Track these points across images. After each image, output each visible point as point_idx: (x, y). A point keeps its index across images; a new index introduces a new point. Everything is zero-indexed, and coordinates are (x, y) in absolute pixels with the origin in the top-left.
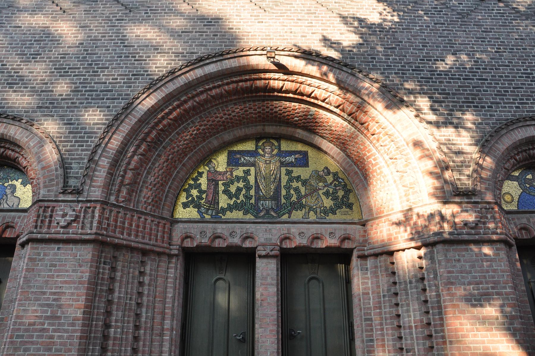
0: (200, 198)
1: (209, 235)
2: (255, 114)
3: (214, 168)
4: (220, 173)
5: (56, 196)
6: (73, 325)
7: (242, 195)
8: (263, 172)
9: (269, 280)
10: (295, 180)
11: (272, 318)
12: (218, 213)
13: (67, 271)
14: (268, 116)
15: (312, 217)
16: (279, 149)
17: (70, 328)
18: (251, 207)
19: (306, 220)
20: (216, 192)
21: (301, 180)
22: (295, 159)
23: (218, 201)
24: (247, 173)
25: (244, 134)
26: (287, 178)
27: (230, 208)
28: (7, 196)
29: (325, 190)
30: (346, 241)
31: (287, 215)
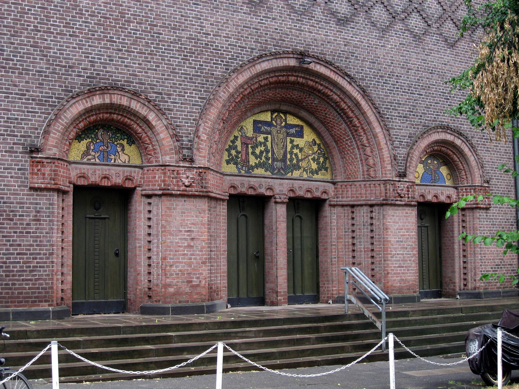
0: (237, 157)
1: (246, 186)
2: (280, 97)
4: (249, 138)
5: (177, 162)
6: (202, 251)
12: (249, 169)
13: (193, 217)
14: (287, 100)
15: (305, 176)
16: (286, 122)
20: (247, 154)
24: (266, 139)
26: (291, 145)
27: (257, 166)
28: (118, 153)
31: (290, 173)
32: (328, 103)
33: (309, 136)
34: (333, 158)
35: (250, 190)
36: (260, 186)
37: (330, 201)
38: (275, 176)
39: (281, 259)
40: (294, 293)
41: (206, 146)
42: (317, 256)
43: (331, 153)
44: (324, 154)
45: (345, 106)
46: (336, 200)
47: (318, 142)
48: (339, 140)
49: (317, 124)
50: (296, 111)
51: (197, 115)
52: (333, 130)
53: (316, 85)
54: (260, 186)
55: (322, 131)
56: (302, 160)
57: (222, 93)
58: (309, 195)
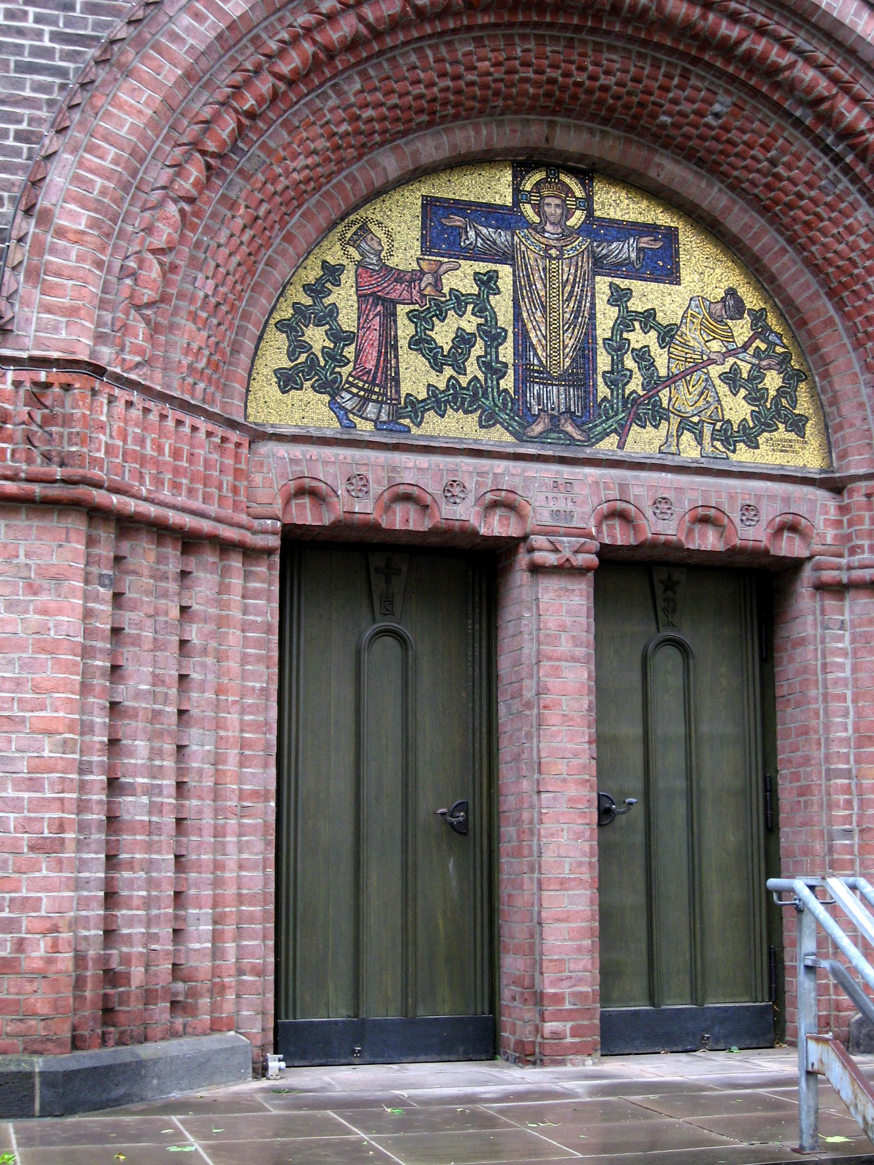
0: (335, 357)
1: (375, 489)
2: (537, 84)
3: (378, 253)
4: (399, 276)
6: (33, 784)
7: (472, 359)
8: (539, 286)
9: (565, 646)
10: (637, 325)
11: (575, 762)
12: (397, 415)
14: (574, 98)
15: (690, 450)
17: (26, 795)
18: (505, 404)
19: (669, 461)
20: (389, 345)
21: (657, 327)
22: (640, 250)
23: (397, 373)
24: (488, 282)
25: (484, 147)
26: (613, 312)
27: (438, 402)
29: (726, 368)
30: (786, 534)
31: (614, 438)
32: (777, 107)
33: (705, 273)
34: (825, 375)
35: (399, 509)
36: (452, 489)
37: (818, 568)
38: (531, 450)
39: (564, 838)
40: (652, 997)
41: (80, 258)
42: (771, 828)
43: (815, 349)
44: (785, 358)
45: (857, 119)
46: (844, 561)
47: (752, 300)
48: (845, 286)
49: (740, 219)
50: (633, 155)
51: (44, 114)
52: (813, 241)
53: (704, 17)
54: (452, 489)
55: (766, 250)
56: (671, 380)
57: (186, 20)
58: (709, 541)
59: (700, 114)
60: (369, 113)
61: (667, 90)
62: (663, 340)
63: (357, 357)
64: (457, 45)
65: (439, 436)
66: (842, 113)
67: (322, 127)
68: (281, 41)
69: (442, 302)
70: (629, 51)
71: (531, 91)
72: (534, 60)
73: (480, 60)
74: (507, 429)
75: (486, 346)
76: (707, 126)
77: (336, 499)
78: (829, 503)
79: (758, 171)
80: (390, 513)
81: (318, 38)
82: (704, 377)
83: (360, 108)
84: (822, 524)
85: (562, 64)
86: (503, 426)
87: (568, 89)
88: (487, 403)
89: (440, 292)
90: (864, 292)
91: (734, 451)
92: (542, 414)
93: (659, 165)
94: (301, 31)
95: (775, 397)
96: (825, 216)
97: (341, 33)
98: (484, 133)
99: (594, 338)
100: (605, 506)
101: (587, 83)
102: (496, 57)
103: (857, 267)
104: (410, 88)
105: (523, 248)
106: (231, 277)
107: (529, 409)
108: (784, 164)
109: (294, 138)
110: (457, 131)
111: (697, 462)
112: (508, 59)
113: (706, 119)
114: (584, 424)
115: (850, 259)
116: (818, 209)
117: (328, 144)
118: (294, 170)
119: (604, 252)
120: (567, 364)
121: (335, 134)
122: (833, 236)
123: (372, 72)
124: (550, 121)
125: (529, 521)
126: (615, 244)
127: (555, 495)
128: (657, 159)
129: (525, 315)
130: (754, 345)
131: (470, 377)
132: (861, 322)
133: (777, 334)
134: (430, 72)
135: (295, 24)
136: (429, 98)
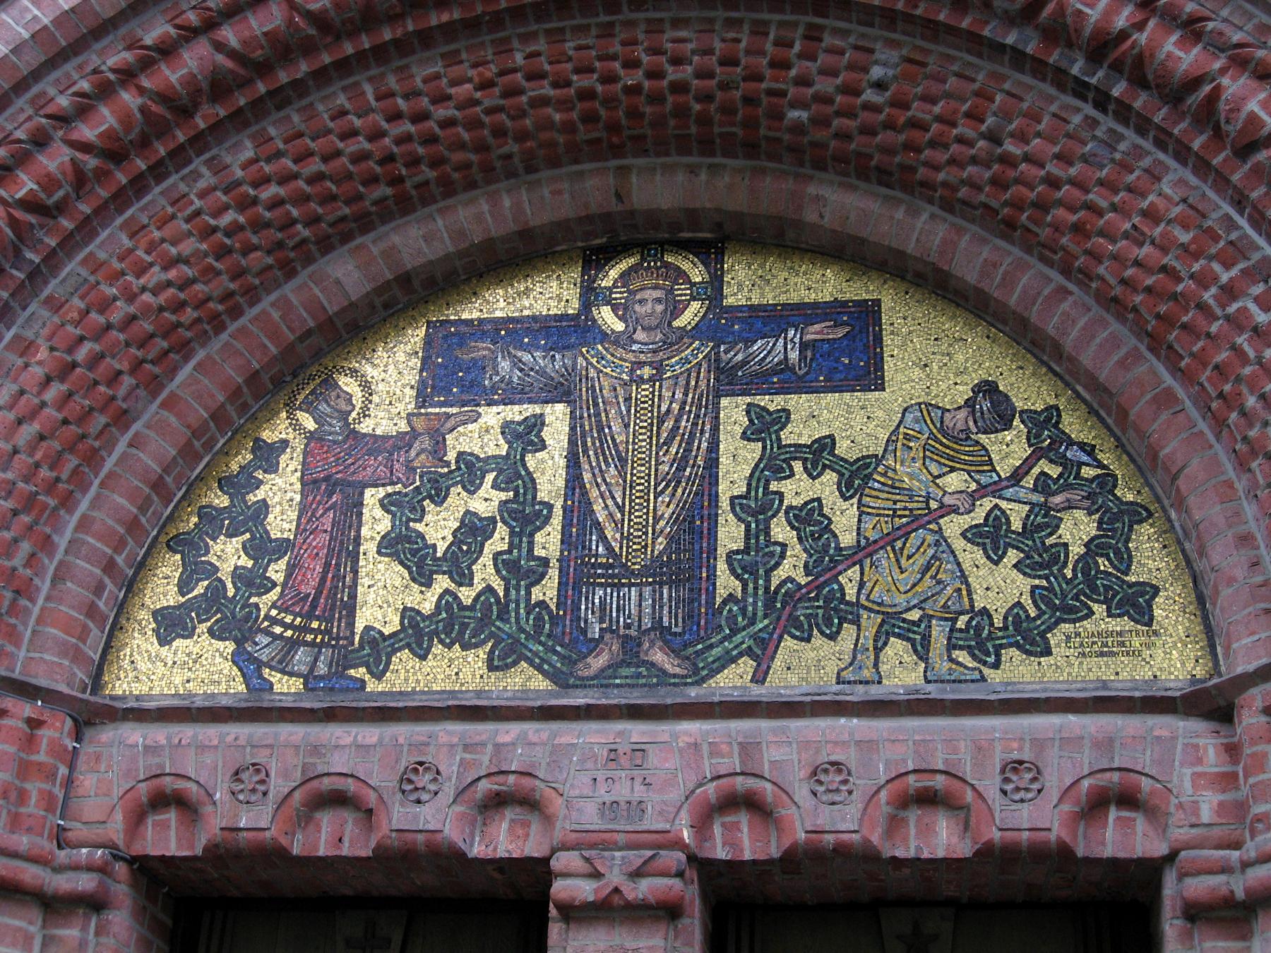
0: (252, 581)
1: (278, 786)
7: (486, 559)
10: (798, 466)
14: (634, 114)
15: (901, 671)
20: (345, 551)
22: (804, 346)
23: (353, 596)
24: (526, 436)
25: (512, 227)
26: (754, 451)
29: (979, 516)
30: (1113, 813)
31: (746, 666)
33: (931, 361)
35: (326, 820)
47: (1028, 391)
49: (975, 256)
50: (766, 192)
56: (863, 551)
59: (851, 90)
60: (273, 190)
61: (786, 65)
62: (849, 485)
63: (289, 575)
64: (414, 70)
65: (414, 692)
66: (1080, 12)
67: (188, 220)
68: (76, 94)
69: (442, 475)
70: (711, 21)
71: (557, 117)
72: (547, 67)
73: (454, 83)
74: (539, 668)
75: (512, 533)
76: (867, 106)
77: (210, 808)
78: (1201, 742)
79: (974, 160)
80: (311, 827)
81: (146, 83)
82: (930, 539)
83: (256, 185)
84: (1187, 784)
85: (597, 64)
86: (531, 664)
87: (620, 101)
88: (507, 627)
89: (441, 460)
90: (1201, 322)
91: (996, 665)
92: (607, 636)
93: (818, 198)
94: (112, 77)
95: (1081, 558)
96: (1104, 204)
97: (185, 71)
98: (507, 203)
99: (714, 498)
100: (711, 788)
101: (646, 84)
102: (480, 74)
103: (1179, 280)
104: (341, 145)
105: (592, 373)
106: (23, 456)
107: (584, 632)
108: (1012, 135)
109: (138, 242)
110: (460, 207)
111: (917, 692)
112: (502, 73)
113: (864, 97)
114: (686, 645)
115: (1164, 269)
116: (1091, 196)
117: (204, 246)
118: (144, 289)
119: (740, 357)
120: (659, 548)
121: (215, 230)
122: (1126, 235)
123: (272, 131)
124: (620, 168)
125: (558, 825)
126: (759, 343)
127: (610, 774)
128: (812, 190)
129: (587, 476)
130: (1036, 471)
131: (479, 586)
132: (1209, 379)
133: (1082, 446)
134: (371, 116)
135: (104, 68)
136: (378, 155)
